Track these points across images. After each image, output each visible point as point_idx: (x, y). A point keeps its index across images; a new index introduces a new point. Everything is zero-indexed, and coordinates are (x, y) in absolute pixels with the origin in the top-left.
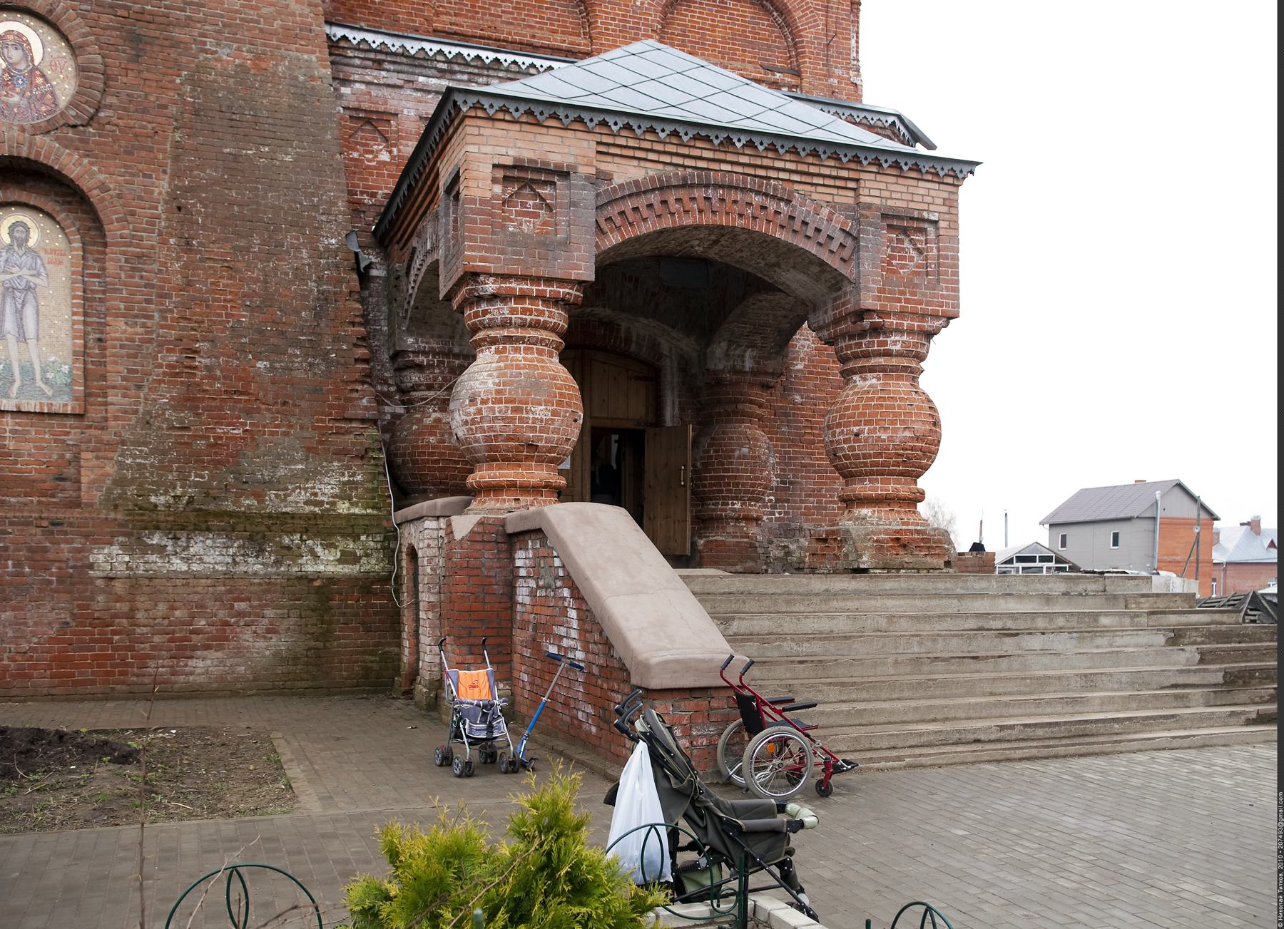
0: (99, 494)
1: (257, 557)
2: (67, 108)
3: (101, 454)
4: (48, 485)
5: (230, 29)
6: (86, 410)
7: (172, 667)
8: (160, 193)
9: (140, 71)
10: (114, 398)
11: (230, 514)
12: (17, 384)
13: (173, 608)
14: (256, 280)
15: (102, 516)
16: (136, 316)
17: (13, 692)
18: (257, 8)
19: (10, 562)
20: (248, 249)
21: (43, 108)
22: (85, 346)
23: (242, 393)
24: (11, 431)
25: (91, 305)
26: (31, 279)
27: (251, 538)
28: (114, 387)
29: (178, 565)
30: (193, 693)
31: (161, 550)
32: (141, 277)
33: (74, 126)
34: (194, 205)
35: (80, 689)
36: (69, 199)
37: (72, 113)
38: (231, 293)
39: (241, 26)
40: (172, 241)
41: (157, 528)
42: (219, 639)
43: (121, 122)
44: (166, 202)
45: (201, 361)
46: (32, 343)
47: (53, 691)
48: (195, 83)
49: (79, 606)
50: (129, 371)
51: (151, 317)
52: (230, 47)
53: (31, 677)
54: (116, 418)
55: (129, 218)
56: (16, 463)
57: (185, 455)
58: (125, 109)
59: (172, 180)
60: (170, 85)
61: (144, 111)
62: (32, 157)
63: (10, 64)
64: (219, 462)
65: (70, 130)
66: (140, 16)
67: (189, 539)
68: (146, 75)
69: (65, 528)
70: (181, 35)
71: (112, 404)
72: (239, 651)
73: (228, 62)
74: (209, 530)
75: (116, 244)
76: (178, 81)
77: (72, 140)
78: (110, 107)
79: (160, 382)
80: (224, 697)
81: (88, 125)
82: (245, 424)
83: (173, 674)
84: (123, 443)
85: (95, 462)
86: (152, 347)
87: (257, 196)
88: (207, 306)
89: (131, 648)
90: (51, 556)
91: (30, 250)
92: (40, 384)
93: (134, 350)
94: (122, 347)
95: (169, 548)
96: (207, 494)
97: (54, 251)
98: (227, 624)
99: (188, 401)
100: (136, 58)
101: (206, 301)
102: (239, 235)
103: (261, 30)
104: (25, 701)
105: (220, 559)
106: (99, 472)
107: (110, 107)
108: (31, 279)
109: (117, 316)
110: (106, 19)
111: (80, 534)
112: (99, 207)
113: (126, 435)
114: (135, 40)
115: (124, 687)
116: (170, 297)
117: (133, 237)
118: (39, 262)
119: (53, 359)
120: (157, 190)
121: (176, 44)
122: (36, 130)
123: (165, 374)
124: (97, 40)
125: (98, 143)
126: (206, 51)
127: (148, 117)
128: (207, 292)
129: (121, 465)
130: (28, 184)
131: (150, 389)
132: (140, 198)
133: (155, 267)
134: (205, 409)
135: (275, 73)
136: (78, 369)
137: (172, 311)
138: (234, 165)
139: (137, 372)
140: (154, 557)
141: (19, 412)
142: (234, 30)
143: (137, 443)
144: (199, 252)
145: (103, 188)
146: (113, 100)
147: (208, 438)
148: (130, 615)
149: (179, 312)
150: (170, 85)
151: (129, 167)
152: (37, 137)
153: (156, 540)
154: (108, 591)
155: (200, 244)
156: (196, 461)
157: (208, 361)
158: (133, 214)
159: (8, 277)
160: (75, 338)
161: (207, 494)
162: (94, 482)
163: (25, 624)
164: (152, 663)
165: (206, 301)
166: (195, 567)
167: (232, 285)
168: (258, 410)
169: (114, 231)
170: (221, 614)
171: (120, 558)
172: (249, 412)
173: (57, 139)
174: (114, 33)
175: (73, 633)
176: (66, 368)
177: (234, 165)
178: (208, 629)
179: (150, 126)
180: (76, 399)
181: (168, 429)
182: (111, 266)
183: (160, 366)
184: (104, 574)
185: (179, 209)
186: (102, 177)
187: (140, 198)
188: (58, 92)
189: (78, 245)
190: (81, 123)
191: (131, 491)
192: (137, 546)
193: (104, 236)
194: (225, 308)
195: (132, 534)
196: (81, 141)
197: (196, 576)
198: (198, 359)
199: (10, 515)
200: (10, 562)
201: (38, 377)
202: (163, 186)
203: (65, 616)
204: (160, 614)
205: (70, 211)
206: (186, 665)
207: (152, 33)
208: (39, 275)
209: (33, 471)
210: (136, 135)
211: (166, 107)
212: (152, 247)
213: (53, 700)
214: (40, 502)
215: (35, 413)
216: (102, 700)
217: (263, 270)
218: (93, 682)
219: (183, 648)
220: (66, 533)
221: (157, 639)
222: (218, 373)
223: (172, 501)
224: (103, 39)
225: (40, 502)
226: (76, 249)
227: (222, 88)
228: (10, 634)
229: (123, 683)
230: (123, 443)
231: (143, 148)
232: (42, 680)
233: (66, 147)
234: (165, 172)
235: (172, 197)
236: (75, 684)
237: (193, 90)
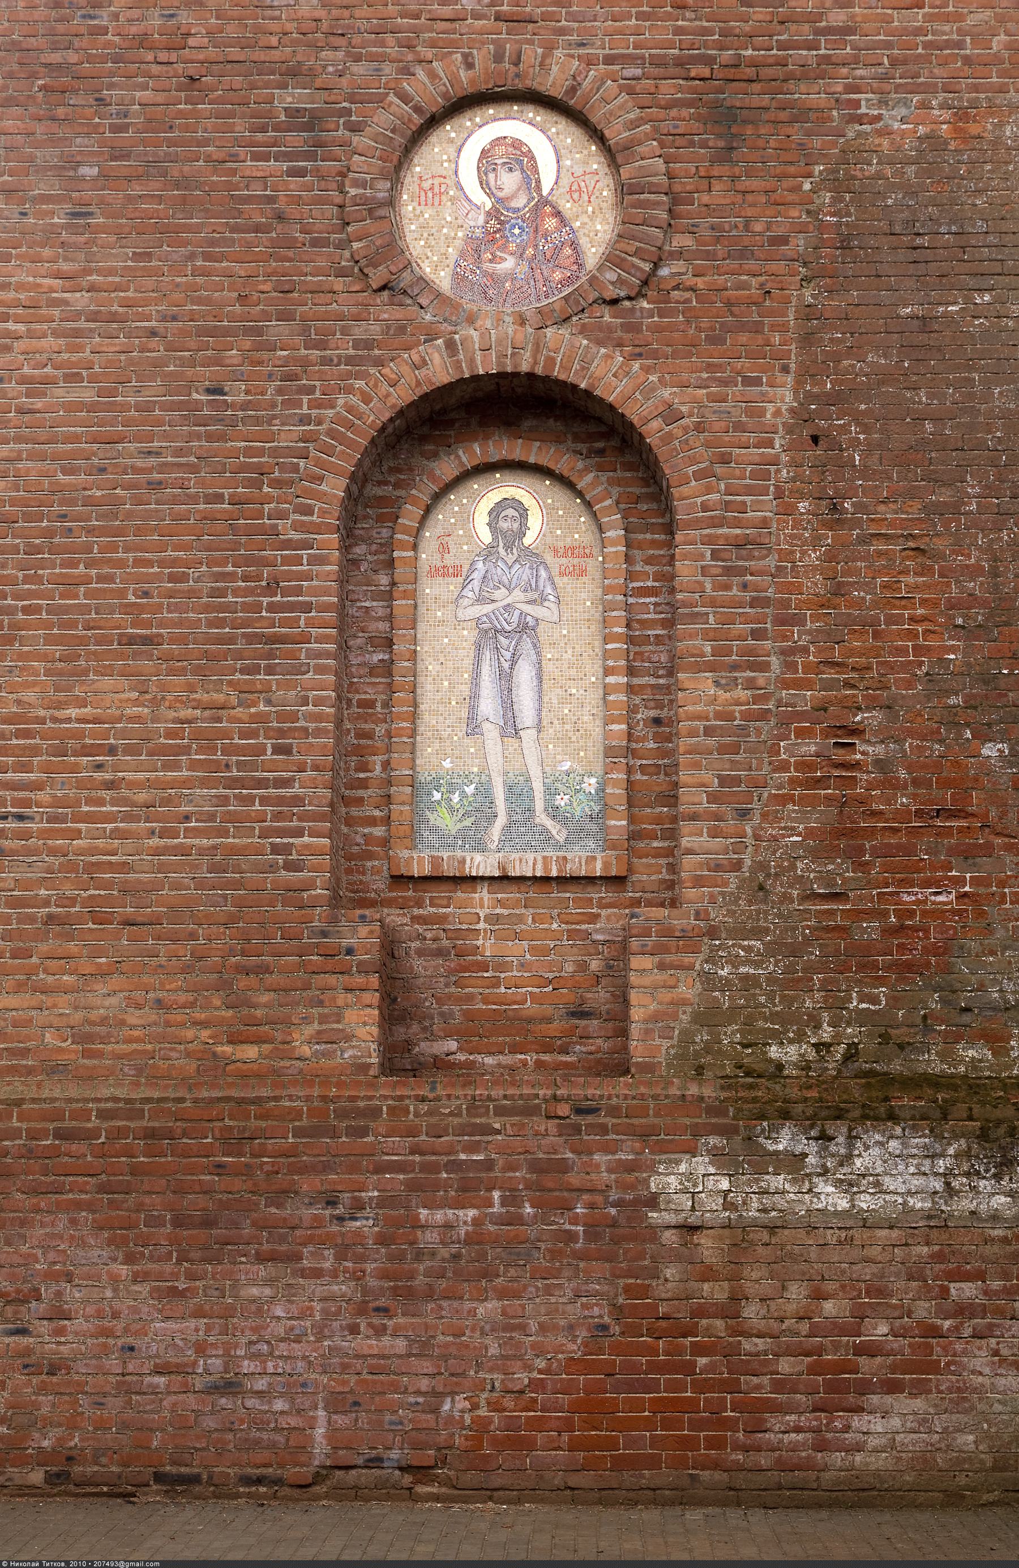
0: (666, 1043)
1: (998, 1177)
2: (600, 268)
3: (669, 958)
4: (555, 1027)
5: (904, 70)
6: (630, 870)
7: (817, 1431)
8: (777, 413)
9: (734, 178)
10: (694, 838)
11: (935, 1082)
12: (501, 821)
13: (818, 1296)
14: (975, 572)
15: (674, 1091)
16: (735, 667)
17: (497, 1481)
18: (959, 17)
19: (496, 1195)
20: (955, 509)
21: (558, 276)
22: (630, 735)
23: (952, 815)
24: (488, 919)
25: (647, 652)
26: (528, 608)
27: (983, 1136)
28: (694, 817)
29: (830, 1197)
30: (861, 1495)
31: (793, 1163)
32: (745, 586)
33: (614, 302)
34: (844, 429)
35: (627, 1477)
36: (600, 445)
37: (611, 276)
38: (923, 602)
39: (926, 59)
40: (803, 506)
41: (785, 1115)
42: (918, 1369)
43: (700, 282)
44: (789, 430)
45: (867, 750)
46: (528, 736)
47: (574, 1480)
48: (838, 185)
49: (627, 1289)
50: (723, 781)
51: (765, 667)
52: (906, 104)
53: (530, 1445)
54: (698, 882)
55: (719, 469)
56: (496, 983)
57: (837, 953)
58: (710, 256)
59: (799, 383)
60: (791, 197)
61: (744, 254)
62: (539, 371)
63: (500, 200)
64: (909, 967)
65: (606, 310)
66: (731, 73)
67: (851, 1138)
68: (745, 183)
69: (602, 1119)
70: (811, 95)
71: (690, 852)
72: (962, 1398)
73: (903, 134)
74: (892, 1117)
75: (696, 524)
76: (807, 187)
77: (610, 329)
78: (679, 254)
79: (784, 800)
80: (930, 1506)
81: (640, 295)
82: (960, 881)
83: (821, 1446)
84: (712, 933)
85: (659, 977)
86: (767, 728)
87: (971, 396)
88: (877, 635)
89: (731, 1386)
90: (574, 1179)
91: (528, 553)
92: (542, 818)
93: (730, 735)
94: (708, 732)
95: (811, 1160)
96: (885, 1038)
97: (570, 551)
98: (934, 1332)
99: (841, 838)
100: (726, 155)
101: (874, 622)
102: (935, 480)
103: (967, 60)
104: (519, 1501)
105: (917, 1182)
106: (666, 996)
107: (679, 254)
108: (528, 608)
109: (698, 668)
110: (669, 90)
111: (631, 1131)
112: (661, 452)
113: (718, 915)
114: (725, 120)
115: (719, 1476)
116: (800, 621)
117: (727, 506)
118: (543, 573)
119: (566, 766)
120: (770, 408)
121: (801, 114)
122: (547, 318)
123: (792, 781)
124: (655, 129)
125: (657, 329)
126: (860, 120)
127: (751, 265)
128: (875, 604)
129: (708, 980)
130: (527, 424)
131: (764, 816)
132: (739, 427)
133: (771, 562)
134: (875, 853)
135: (997, 143)
136: (615, 783)
137: (805, 650)
138: (923, 338)
139: (737, 781)
140: (778, 1182)
141: (504, 879)
142: (912, 68)
143: (740, 933)
144: (857, 523)
145: (671, 415)
146: (681, 241)
147: (885, 914)
148: (731, 1310)
149: (820, 651)
150: (791, 197)
151: (719, 368)
152: (549, 332)
153: (784, 1141)
154: (686, 1256)
155: (859, 507)
156: (862, 967)
157: (880, 749)
158: (725, 460)
159: (488, 608)
160: (608, 721)
161: (885, 1038)
162: (655, 1018)
163: (523, 1328)
164: (774, 1421)
165: (874, 622)
166: (865, 1202)
167: (927, 586)
168: (988, 850)
169: (690, 497)
170: (923, 1309)
171: (710, 1184)
172: (968, 854)
173: (583, 330)
174: (685, 112)
175: (617, 1349)
176: (591, 784)
177: (923, 338)
178: (896, 1343)
179: (754, 282)
180: (610, 845)
181: (804, 898)
182: (685, 570)
183: (784, 767)
184: (680, 1219)
185: (815, 439)
186: (666, 393)
187: (739, 427)
188: (583, 241)
189: (615, 533)
190: (623, 297)
191: (731, 1035)
192: (746, 1158)
193: (668, 510)
194: (913, 635)
195: (736, 1131)
196: (628, 328)
197: (867, 1222)
198: (861, 747)
199: (497, 1092)
200: (496, 1195)
201: (539, 805)
202: (783, 397)
203: (601, 1313)
204: (791, 1308)
205: (600, 468)
206: (847, 1429)
207: (756, 101)
208: (543, 599)
209: (526, 997)
210: (729, 303)
211: (784, 240)
212: (765, 523)
213: (574, 1501)
214: (539, 1064)
215: (534, 878)
216: (672, 1503)
217: (988, 549)
218: (653, 1462)
219: (840, 1389)
220: (604, 1130)
221: (785, 1365)
222: (903, 774)
223: (812, 1055)
224: (666, 126)
225: (539, 1064)
226: (614, 544)
227: (893, 188)
228: (494, 1350)
229: (716, 1465)
230: (712, 933)
231: (742, 327)
232: (552, 1454)
233: (600, 343)
234: (785, 369)
235: (801, 416)
236: (620, 1464)
237: (836, 200)
